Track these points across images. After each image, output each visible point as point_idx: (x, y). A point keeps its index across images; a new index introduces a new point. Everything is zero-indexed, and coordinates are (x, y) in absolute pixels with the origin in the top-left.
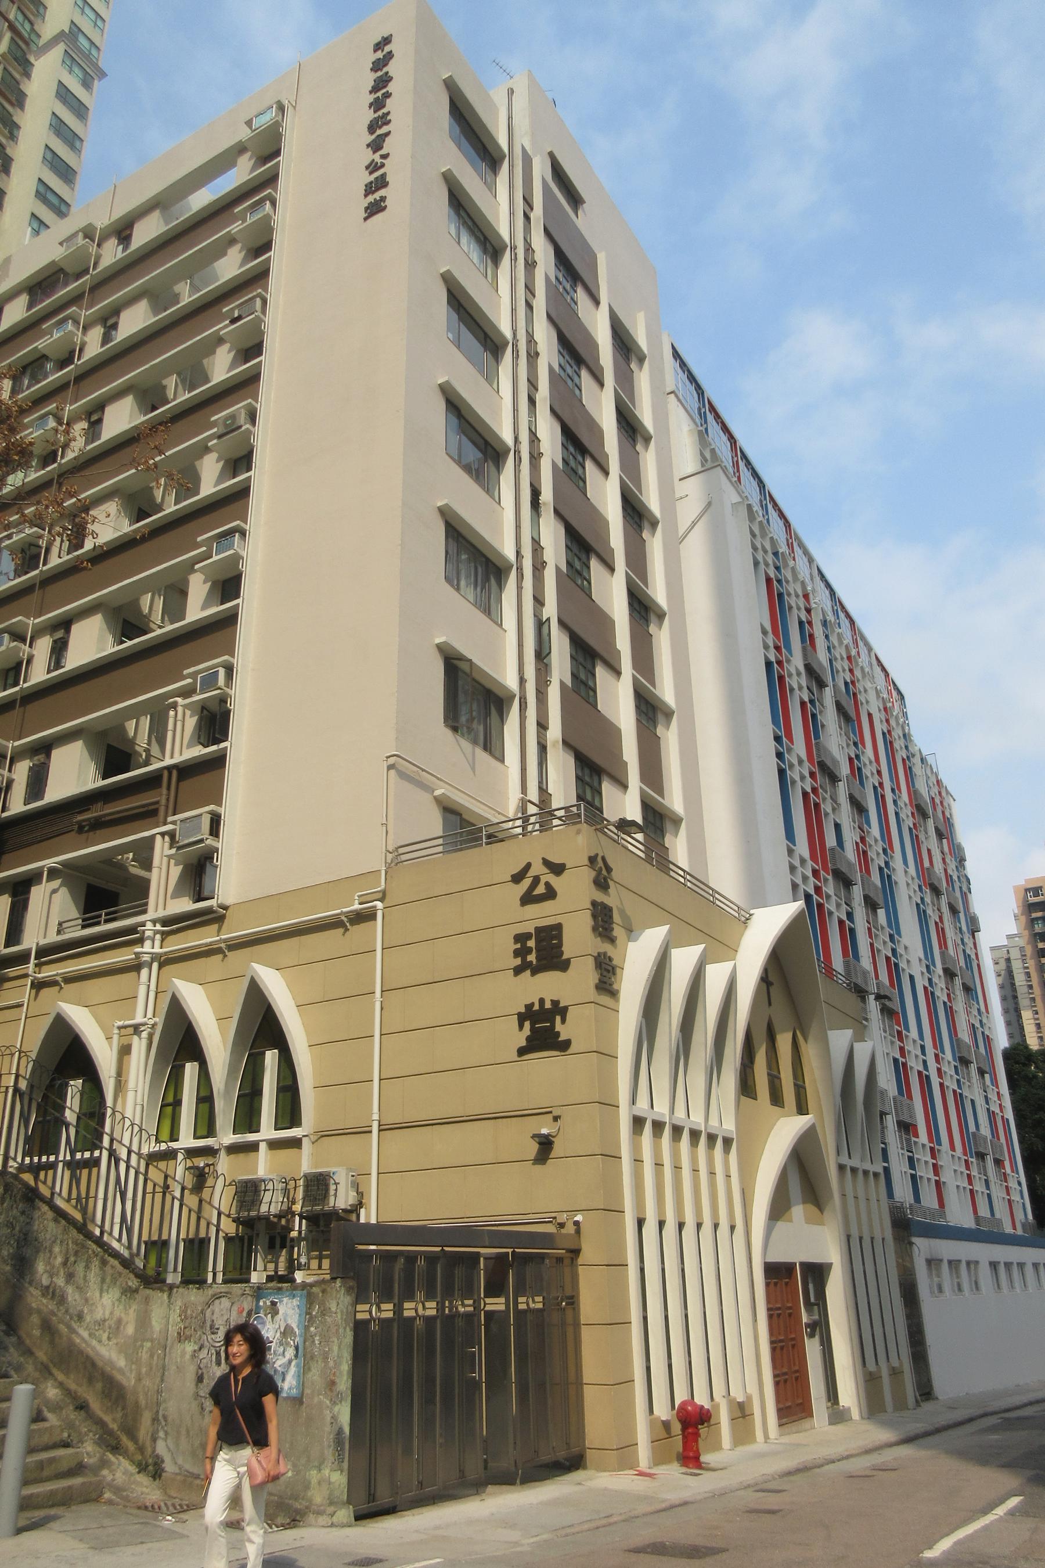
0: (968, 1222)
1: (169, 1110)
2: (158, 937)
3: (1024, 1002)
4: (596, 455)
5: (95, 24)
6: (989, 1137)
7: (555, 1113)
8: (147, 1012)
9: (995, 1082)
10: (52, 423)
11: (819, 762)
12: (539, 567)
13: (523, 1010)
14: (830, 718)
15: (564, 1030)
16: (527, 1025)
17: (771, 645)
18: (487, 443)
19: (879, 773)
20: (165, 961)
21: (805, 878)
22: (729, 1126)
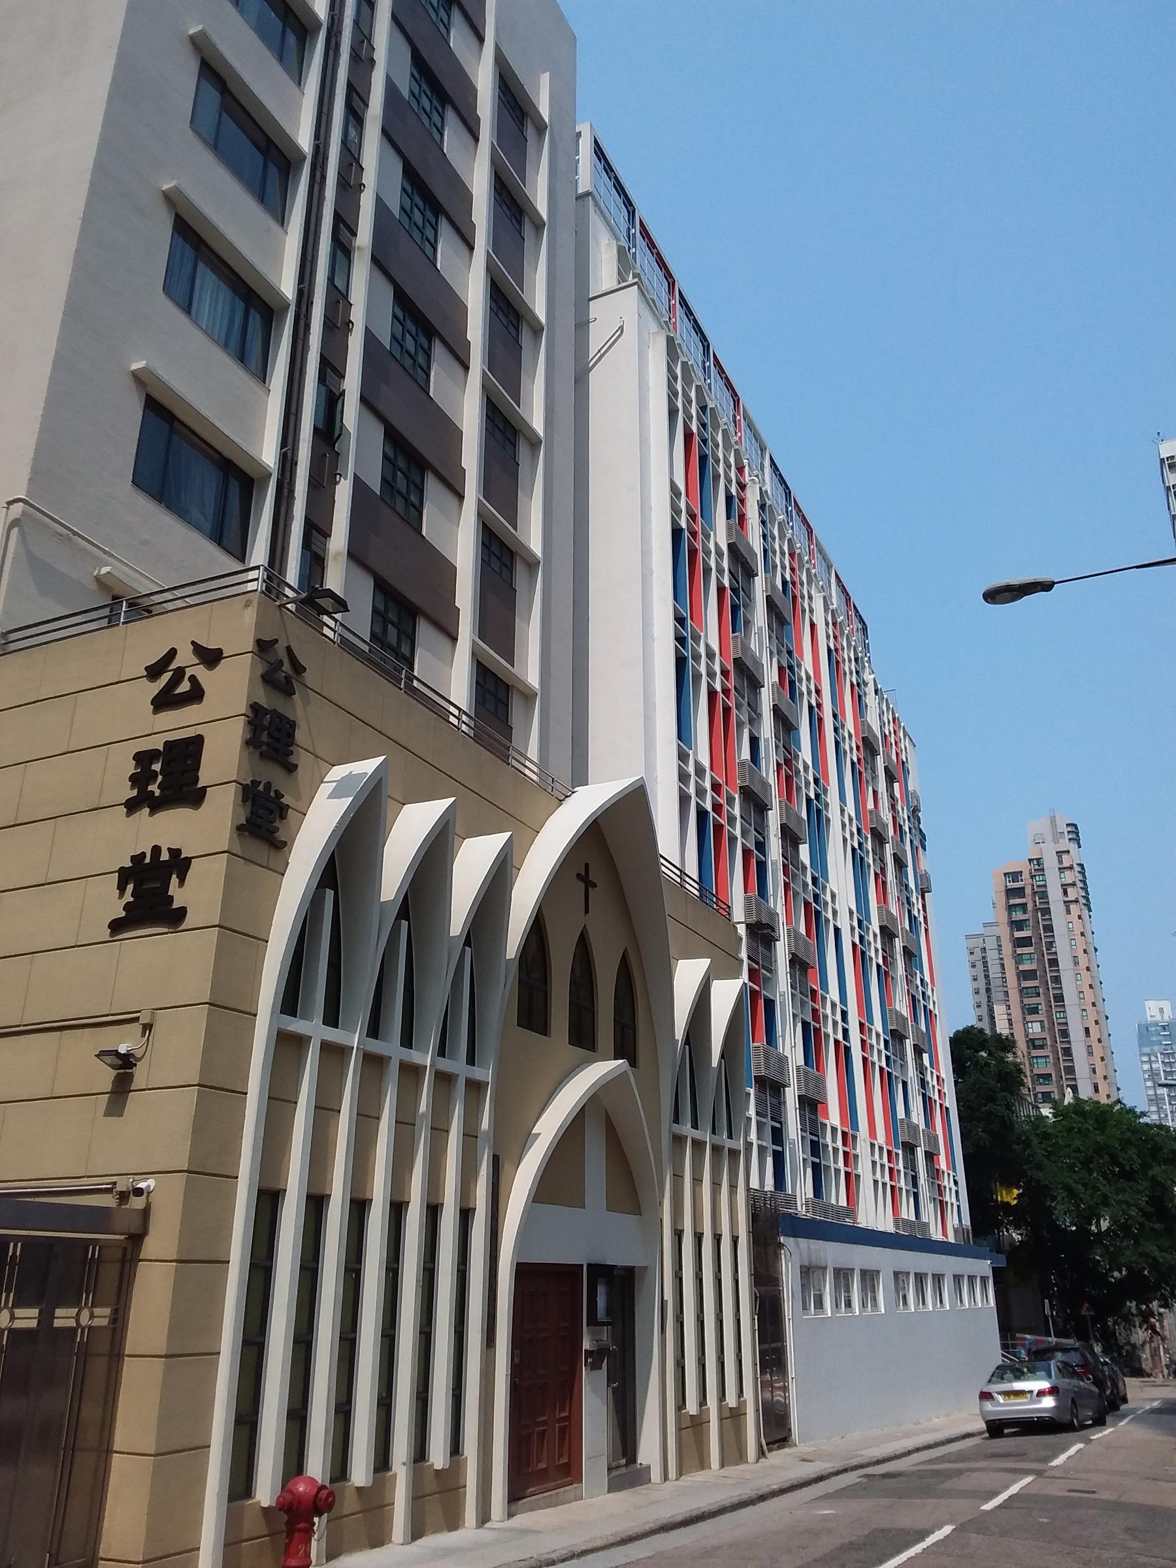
0: (886, 1225)
3: (997, 995)
4: (452, 214)
6: (922, 1126)
9: (934, 1062)
15: (179, 895)
18: (270, 142)
19: (818, 692)
21: (700, 792)
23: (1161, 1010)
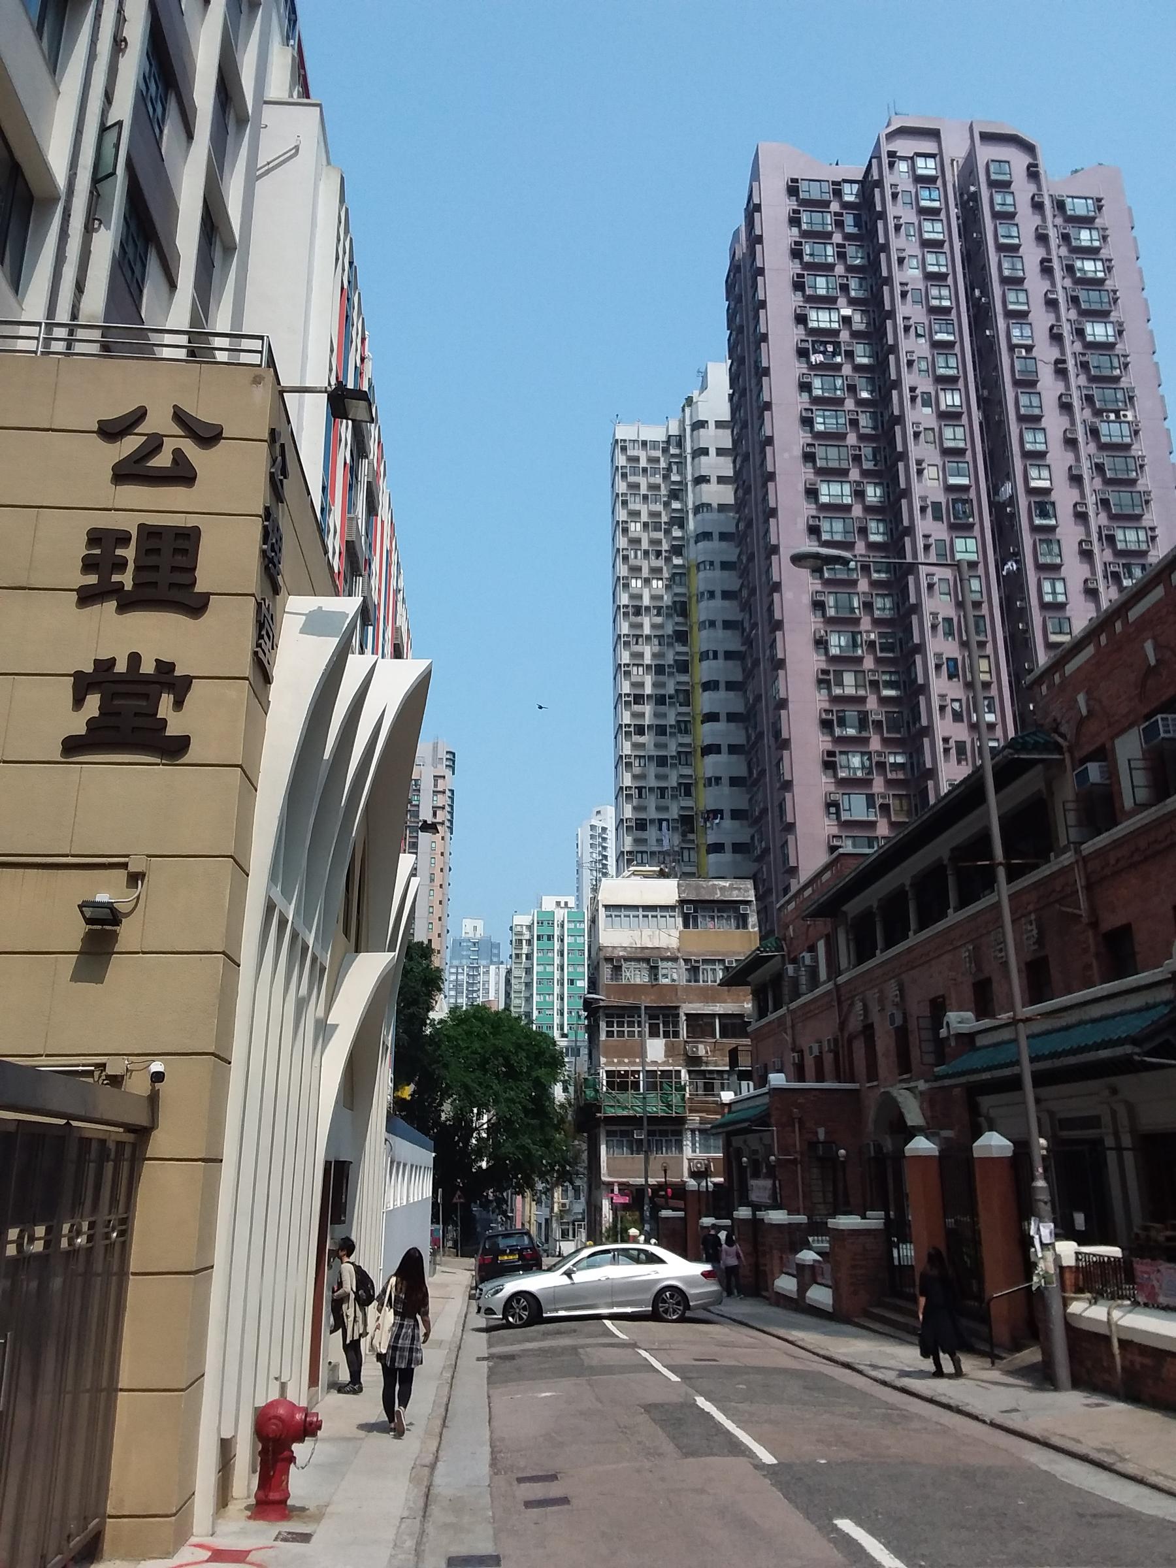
7: (132, 868)
13: (89, 668)
16: (93, 704)
23: (475, 928)
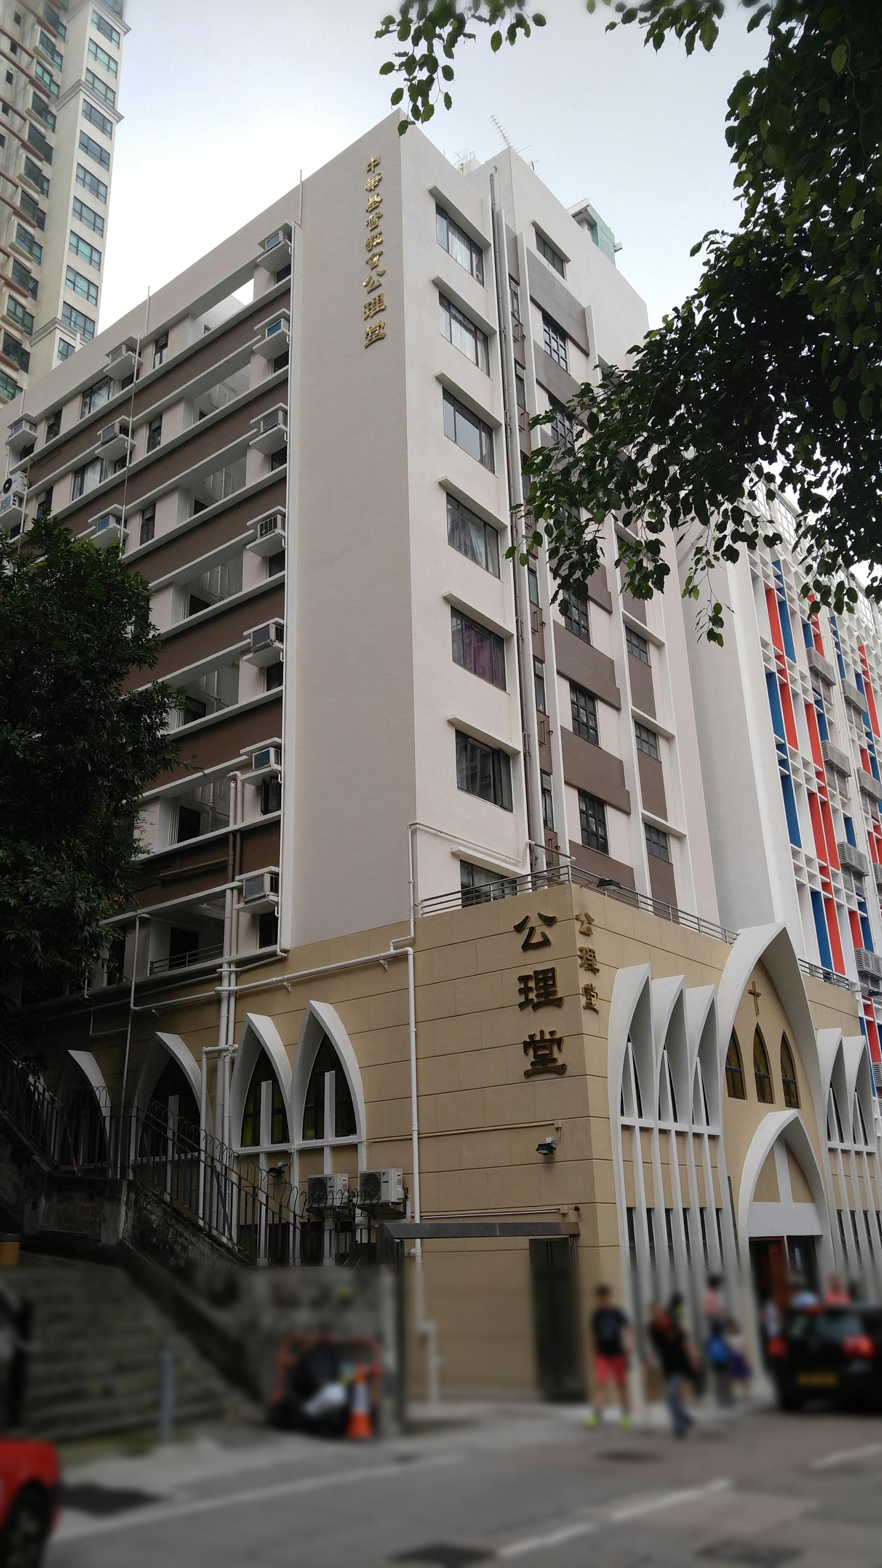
1: (250, 1120)
2: (233, 976)
5: (109, 67)
8: (227, 1039)
10: (112, 523)
11: (826, 762)
12: (539, 626)
14: (838, 713)
15: (561, 1058)
16: (531, 1052)
17: (773, 656)
20: (240, 996)
21: (811, 877)
22: (715, 1129)
